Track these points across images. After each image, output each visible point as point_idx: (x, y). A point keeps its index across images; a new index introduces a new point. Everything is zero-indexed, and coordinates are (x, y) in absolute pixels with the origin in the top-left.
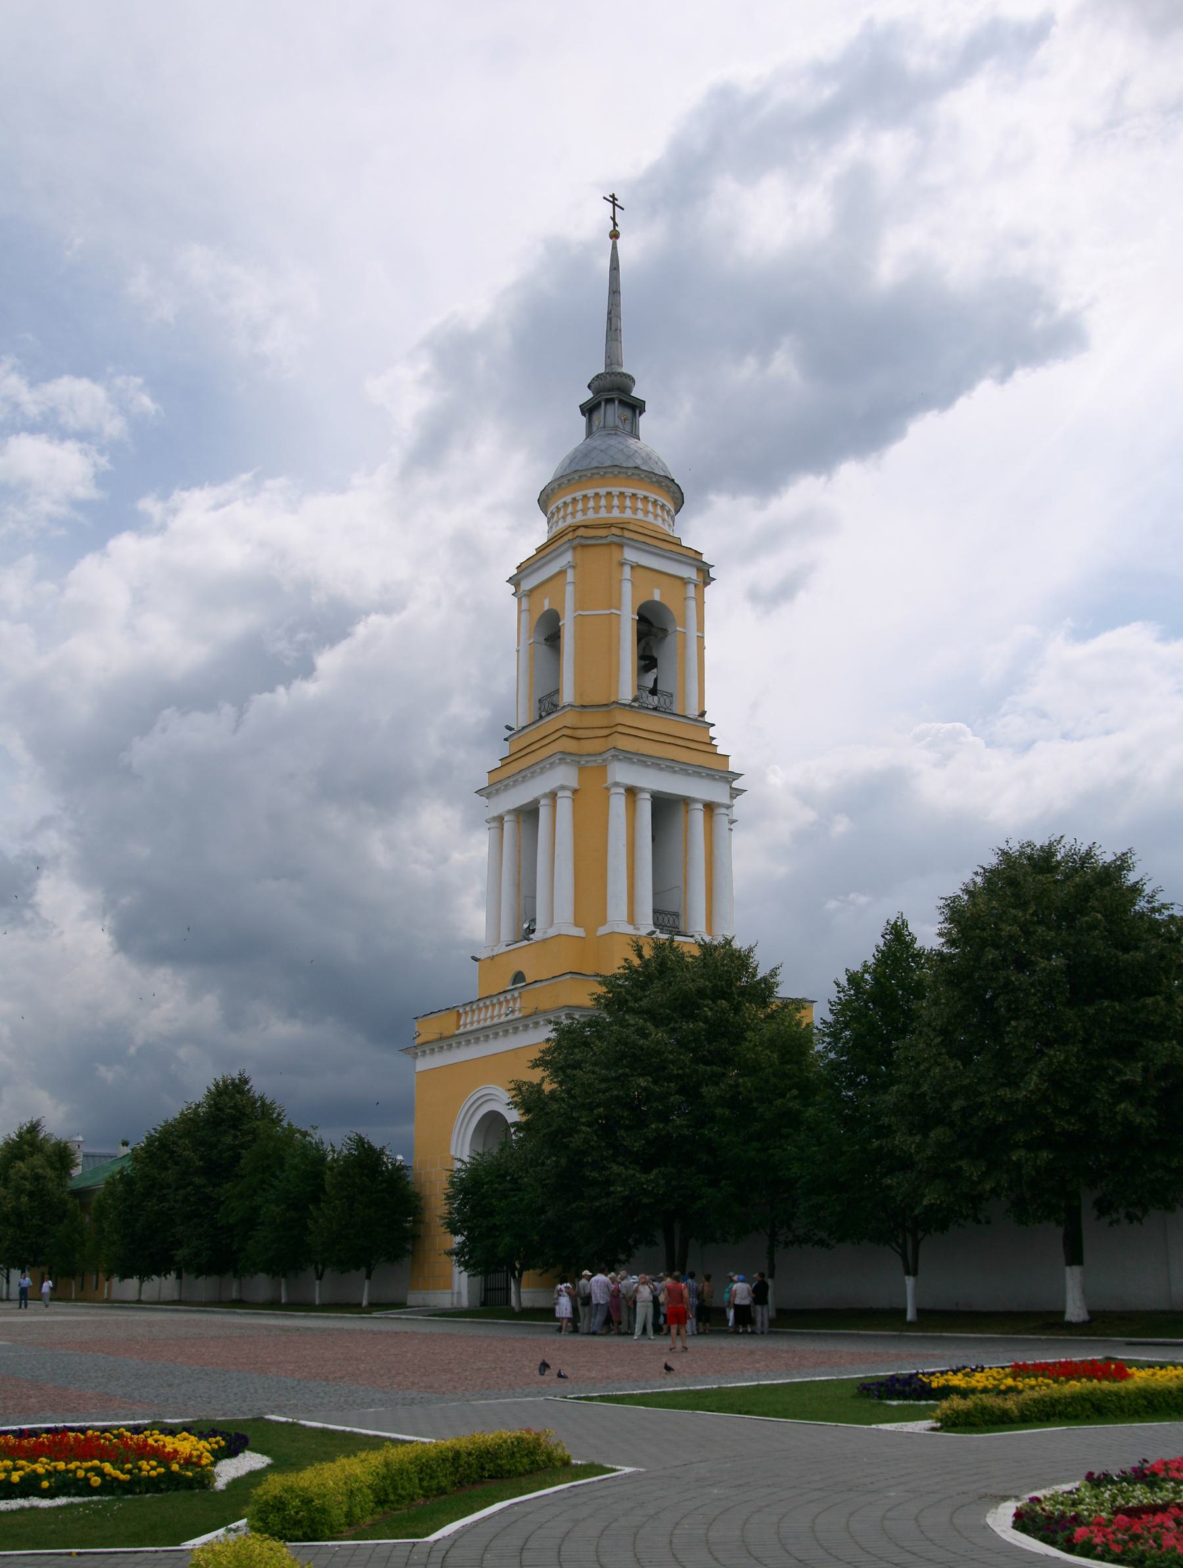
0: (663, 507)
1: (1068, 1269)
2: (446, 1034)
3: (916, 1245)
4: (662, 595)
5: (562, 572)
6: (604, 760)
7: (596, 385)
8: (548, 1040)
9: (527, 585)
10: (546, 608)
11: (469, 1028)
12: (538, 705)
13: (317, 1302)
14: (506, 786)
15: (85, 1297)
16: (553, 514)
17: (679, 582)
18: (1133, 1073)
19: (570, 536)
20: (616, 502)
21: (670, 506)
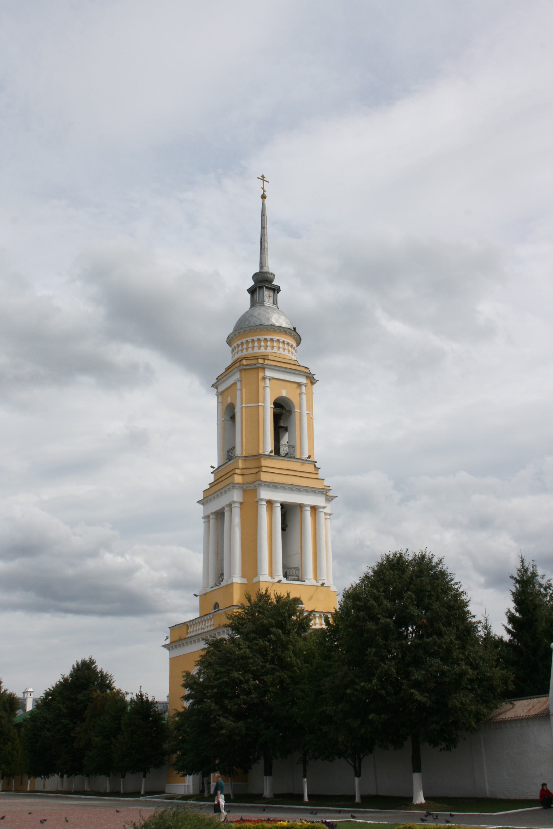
0: (288, 344)
1: (265, 777)
2: (182, 637)
3: (360, 760)
4: (287, 393)
5: (235, 384)
6: (255, 486)
7: (256, 277)
8: (203, 650)
9: (222, 388)
10: (229, 402)
11: (192, 634)
12: (227, 454)
13: (122, 792)
14: (214, 497)
15: (20, 790)
16: (235, 348)
17: (296, 385)
18: (417, 675)
19: (237, 365)
20: (262, 343)
21: (294, 343)
